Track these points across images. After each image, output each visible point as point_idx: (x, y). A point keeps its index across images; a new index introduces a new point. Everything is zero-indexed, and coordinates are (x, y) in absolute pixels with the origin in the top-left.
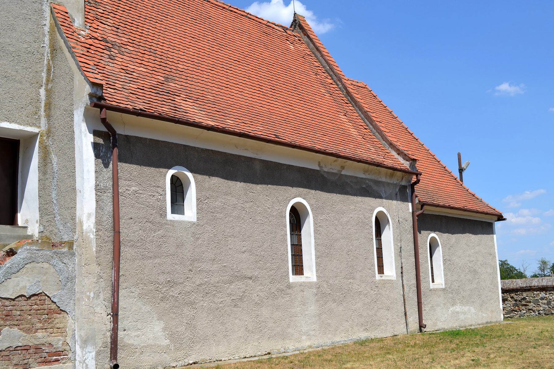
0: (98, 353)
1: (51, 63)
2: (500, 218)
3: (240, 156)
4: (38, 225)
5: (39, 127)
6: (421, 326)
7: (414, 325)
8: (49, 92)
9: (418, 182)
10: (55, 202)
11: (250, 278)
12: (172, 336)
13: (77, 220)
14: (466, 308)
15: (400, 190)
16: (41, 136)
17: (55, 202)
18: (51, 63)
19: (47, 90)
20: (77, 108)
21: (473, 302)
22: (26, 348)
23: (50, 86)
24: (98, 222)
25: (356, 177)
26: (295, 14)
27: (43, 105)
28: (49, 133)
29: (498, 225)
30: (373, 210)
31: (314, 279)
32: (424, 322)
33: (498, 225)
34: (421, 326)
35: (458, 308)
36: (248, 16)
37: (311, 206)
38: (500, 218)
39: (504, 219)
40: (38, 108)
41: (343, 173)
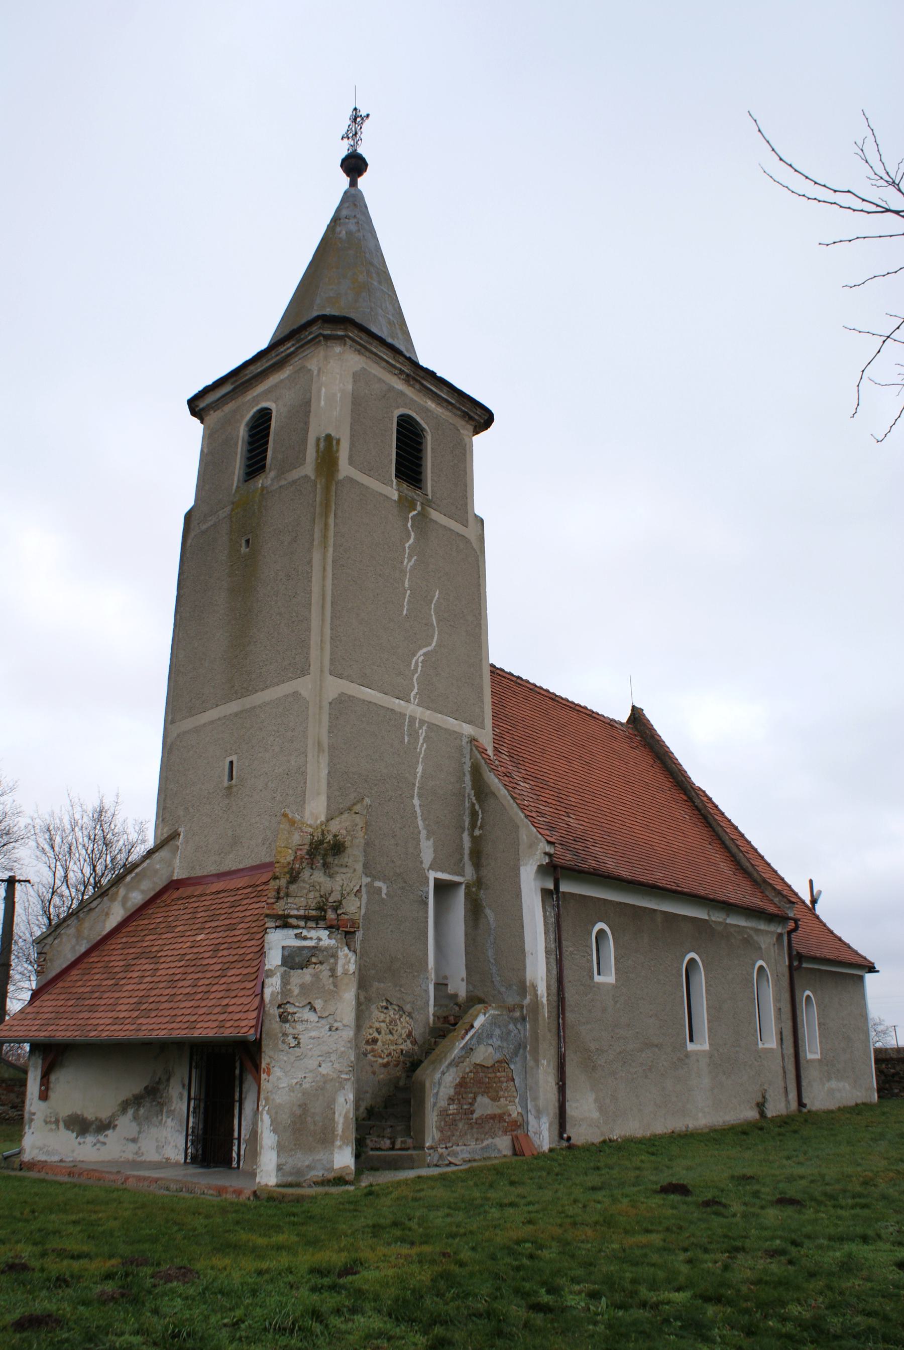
0: (551, 1125)
1: (477, 807)
2: (872, 969)
3: (645, 908)
4: (464, 983)
5: (463, 876)
6: (801, 1104)
7: (794, 1105)
8: (475, 840)
9: (796, 929)
10: (492, 961)
11: (657, 1046)
12: (601, 1109)
13: (528, 984)
14: (841, 1085)
15: (777, 939)
16: (468, 887)
17: (492, 961)
18: (477, 807)
19: (471, 835)
20: (526, 865)
21: (848, 1077)
22: (493, 1117)
23: (477, 833)
24: (548, 987)
25: (739, 926)
26: (633, 707)
27: (467, 852)
28: (479, 883)
29: (869, 977)
30: (754, 965)
31: (706, 1047)
32: (805, 1101)
33: (869, 977)
34: (801, 1104)
35: (833, 1084)
36: (518, 681)
37: (702, 961)
38: (872, 969)
39: (878, 971)
40: (462, 855)
41: (728, 922)
